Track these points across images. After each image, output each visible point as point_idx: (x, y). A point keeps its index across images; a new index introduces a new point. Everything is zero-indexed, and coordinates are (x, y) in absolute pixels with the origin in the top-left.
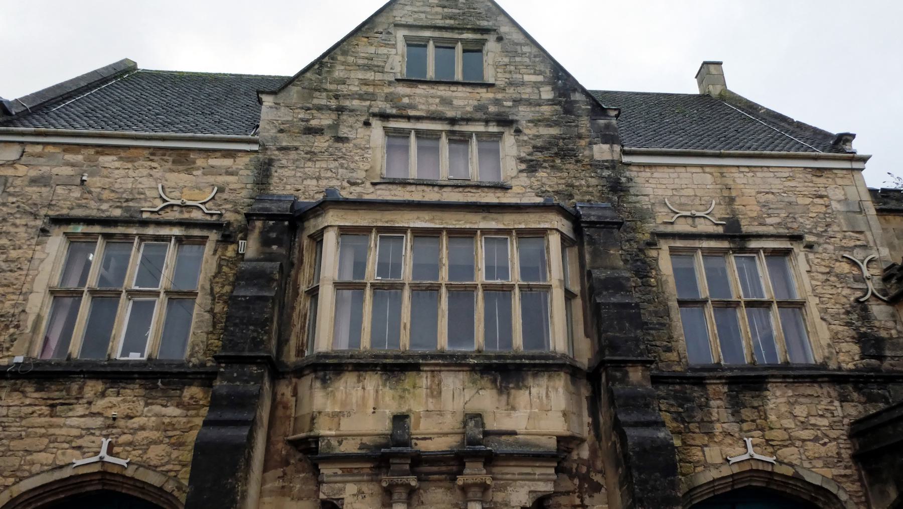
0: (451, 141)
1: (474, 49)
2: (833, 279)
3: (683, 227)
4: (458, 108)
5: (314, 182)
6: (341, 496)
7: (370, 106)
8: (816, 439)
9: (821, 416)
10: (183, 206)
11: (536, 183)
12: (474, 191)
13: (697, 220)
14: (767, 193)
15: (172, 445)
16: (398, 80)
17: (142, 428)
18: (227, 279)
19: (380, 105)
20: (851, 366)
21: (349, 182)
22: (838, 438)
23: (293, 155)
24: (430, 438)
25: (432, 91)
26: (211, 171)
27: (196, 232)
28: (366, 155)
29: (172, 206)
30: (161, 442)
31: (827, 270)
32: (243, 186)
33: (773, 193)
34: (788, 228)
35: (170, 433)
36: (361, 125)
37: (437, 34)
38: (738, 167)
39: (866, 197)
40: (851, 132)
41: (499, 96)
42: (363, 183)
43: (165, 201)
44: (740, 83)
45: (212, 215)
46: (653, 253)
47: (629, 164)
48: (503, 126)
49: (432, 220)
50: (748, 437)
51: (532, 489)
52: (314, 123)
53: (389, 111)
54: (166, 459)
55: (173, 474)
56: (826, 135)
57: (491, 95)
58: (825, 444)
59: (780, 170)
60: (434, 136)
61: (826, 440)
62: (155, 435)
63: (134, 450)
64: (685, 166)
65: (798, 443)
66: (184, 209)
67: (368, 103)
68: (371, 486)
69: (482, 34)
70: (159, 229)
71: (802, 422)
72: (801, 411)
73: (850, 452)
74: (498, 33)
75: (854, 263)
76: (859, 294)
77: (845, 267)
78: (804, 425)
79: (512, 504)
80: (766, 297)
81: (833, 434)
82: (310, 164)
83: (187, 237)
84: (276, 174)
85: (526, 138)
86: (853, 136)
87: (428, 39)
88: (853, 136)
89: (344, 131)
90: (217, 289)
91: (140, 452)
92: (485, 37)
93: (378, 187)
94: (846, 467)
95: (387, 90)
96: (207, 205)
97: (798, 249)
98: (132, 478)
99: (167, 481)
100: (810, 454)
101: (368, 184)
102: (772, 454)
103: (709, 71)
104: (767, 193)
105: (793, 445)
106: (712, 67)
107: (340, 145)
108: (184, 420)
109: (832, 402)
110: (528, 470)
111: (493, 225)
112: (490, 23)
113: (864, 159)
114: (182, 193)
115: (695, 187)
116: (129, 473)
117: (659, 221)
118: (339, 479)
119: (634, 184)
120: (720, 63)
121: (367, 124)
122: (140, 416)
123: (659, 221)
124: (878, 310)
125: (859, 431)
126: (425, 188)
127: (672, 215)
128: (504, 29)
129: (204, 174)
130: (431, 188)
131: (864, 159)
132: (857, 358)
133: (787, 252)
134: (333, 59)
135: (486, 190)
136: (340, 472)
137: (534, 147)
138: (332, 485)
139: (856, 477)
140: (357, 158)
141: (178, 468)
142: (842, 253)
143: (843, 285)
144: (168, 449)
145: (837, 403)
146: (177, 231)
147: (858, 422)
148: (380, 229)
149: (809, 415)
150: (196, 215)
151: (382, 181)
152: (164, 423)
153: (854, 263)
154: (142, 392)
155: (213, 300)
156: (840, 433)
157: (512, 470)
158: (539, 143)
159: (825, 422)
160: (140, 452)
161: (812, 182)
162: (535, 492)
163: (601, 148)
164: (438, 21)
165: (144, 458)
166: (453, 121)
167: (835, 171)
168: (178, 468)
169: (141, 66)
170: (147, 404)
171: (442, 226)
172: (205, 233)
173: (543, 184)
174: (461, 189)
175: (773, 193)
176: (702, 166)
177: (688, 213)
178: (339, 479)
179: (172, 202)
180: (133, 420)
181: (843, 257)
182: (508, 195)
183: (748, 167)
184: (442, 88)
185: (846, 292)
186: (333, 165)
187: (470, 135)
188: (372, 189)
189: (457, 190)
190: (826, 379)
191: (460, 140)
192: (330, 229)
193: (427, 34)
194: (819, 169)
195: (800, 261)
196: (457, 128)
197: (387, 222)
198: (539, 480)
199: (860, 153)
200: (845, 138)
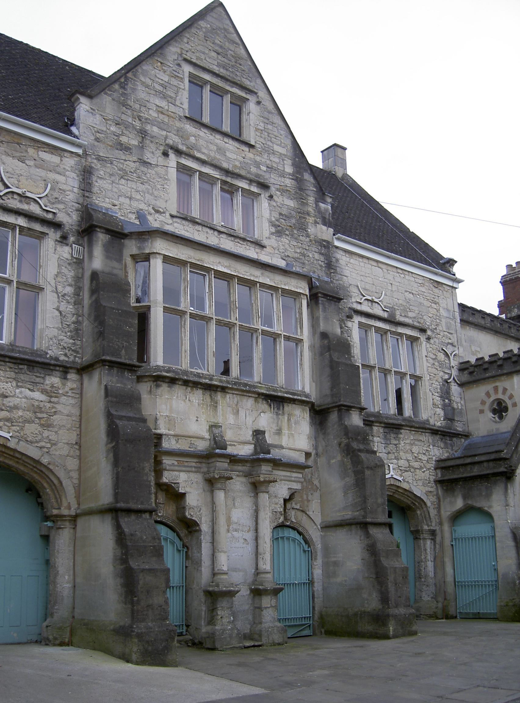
0: (222, 190)
1: (238, 104)
2: (436, 364)
3: (365, 308)
4: (228, 159)
5: (128, 201)
6: (177, 482)
7: (166, 138)
8: (421, 468)
9: (424, 454)
10: (23, 197)
11: (282, 247)
12: (241, 242)
13: (374, 304)
14: (410, 293)
15: (42, 425)
16: (186, 117)
17: (16, 407)
18: (67, 281)
19: (173, 139)
20: (438, 424)
21: (153, 208)
22: (430, 469)
23: (109, 168)
24: (234, 445)
25: (211, 137)
26: (41, 165)
27: (37, 227)
28: (165, 186)
29: (13, 193)
30: (33, 422)
31: (434, 357)
32: (71, 188)
33: (413, 294)
34: (419, 322)
35: (39, 415)
36: (160, 155)
37: (215, 80)
38: (397, 268)
39: (457, 309)
40: (455, 259)
41: (258, 159)
42: (164, 213)
43: (7, 187)
44: (361, 171)
45: (47, 211)
46: (349, 324)
47: (337, 247)
48: (261, 188)
49: (228, 267)
50: (391, 464)
51: (290, 487)
52: (124, 139)
53: (180, 147)
54: (40, 437)
55: (46, 450)
56: (442, 258)
57: (251, 155)
58: (424, 472)
59: (418, 277)
60: (212, 181)
61: (425, 469)
62: (29, 415)
63: (13, 426)
64: (368, 258)
65: (412, 470)
66: (23, 199)
67: (164, 133)
68: (196, 476)
69: (246, 93)
70: (6, 216)
71: (416, 457)
72: (415, 449)
73: (434, 478)
74: (258, 97)
75: (447, 355)
76: (446, 377)
77: (441, 356)
78: (416, 459)
79: (279, 496)
80: (372, 363)
81: (428, 466)
82: (123, 181)
83: (29, 229)
84: (97, 184)
85: (275, 204)
86: (456, 262)
87: (206, 82)
88: (456, 262)
89: (148, 156)
90: (60, 288)
91: (18, 428)
92: (248, 96)
93: (175, 220)
94: (432, 487)
95: (178, 124)
96: (43, 199)
97: (423, 338)
98: (15, 450)
99: (42, 455)
100: (417, 477)
101: (168, 215)
102: (401, 476)
103: (335, 151)
104: (410, 293)
105: (410, 471)
106: (340, 150)
107: (145, 169)
108: (48, 405)
109: (429, 446)
110: (288, 474)
111: (268, 281)
112: (252, 84)
113: (459, 281)
114: (19, 181)
115: (373, 277)
116: (12, 444)
117: (354, 300)
118: (176, 468)
119: (339, 265)
120: (345, 149)
121: (165, 154)
122: (13, 396)
123: (354, 300)
124: (455, 389)
125: (442, 465)
126: (208, 230)
127: (362, 297)
128: (262, 94)
129: (36, 166)
130: (212, 231)
131: (459, 281)
132: (442, 419)
133: (417, 339)
134: (135, 76)
135: (249, 244)
136: (176, 463)
137: (281, 214)
138: (171, 472)
139: (435, 493)
140: (159, 187)
141: (49, 445)
142: (442, 346)
143: (440, 369)
144: (39, 428)
145: (431, 447)
146: (21, 221)
147: (439, 461)
148: (193, 265)
149: (419, 453)
150: (34, 209)
151: (178, 215)
152: (33, 405)
153: (447, 355)
154: (13, 375)
155: (58, 297)
156: (432, 465)
157: (280, 473)
158: (285, 211)
159: (425, 458)
160: (18, 428)
161: (432, 290)
162: (291, 489)
163: (321, 229)
164: (215, 67)
165: (22, 434)
166: (227, 172)
167: (444, 286)
168: (49, 445)
169: (501, 297)
170: (18, 387)
171: (235, 274)
172: (44, 229)
173: (286, 250)
174: (233, 239)
175: (413, 294)
176: (377, 261)
177: (370, 298)
178: (176, 468)
179: (14, 189)
180: (8, 399)
181: (443, 349)
182: (263, 253)
183: (402, 269)
184: (218, 136)
185: (441, 374)
186: (141, 187)
187: (237, 188)
188: (170, 221)
189: (230, 238)
190: (429, 431)
191: (230, 190)
192: (158, 256)
193: (207, 77)
194: (438, 283)
195: (424, 347)
196: (229, 180)
197: (198, 260)
198: (294, 481)
199: (458, 276)
200: (452, 262)
